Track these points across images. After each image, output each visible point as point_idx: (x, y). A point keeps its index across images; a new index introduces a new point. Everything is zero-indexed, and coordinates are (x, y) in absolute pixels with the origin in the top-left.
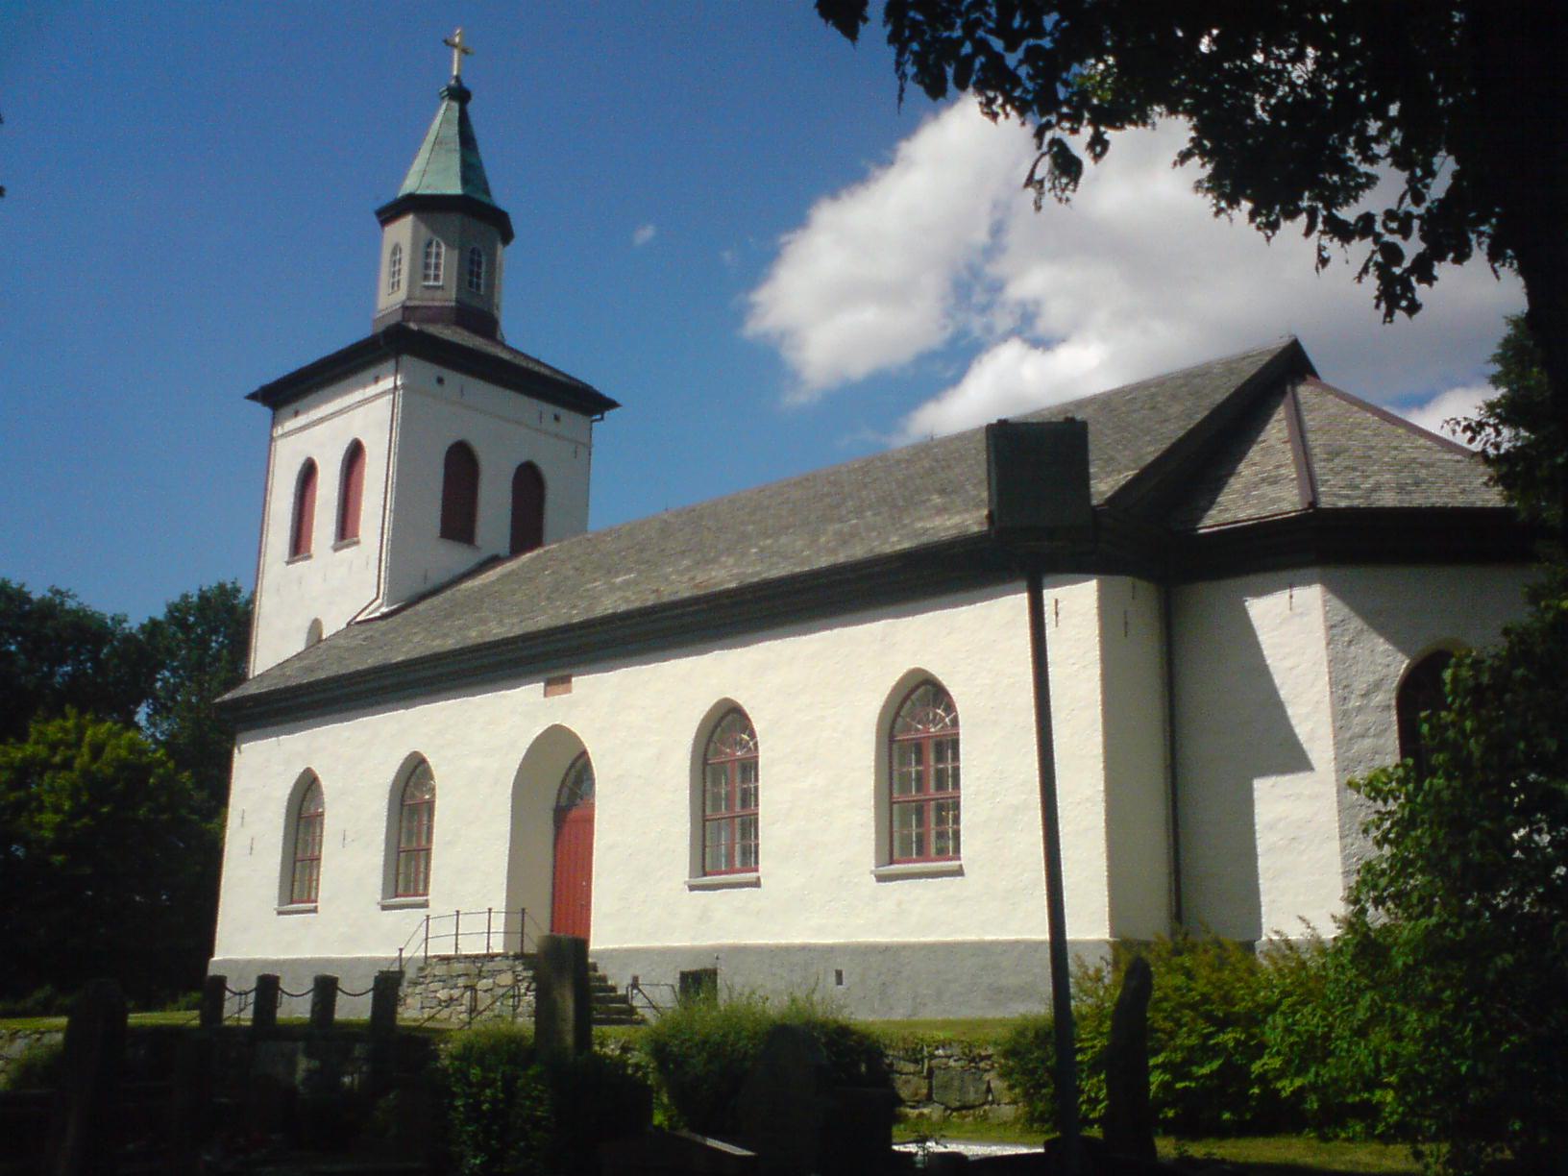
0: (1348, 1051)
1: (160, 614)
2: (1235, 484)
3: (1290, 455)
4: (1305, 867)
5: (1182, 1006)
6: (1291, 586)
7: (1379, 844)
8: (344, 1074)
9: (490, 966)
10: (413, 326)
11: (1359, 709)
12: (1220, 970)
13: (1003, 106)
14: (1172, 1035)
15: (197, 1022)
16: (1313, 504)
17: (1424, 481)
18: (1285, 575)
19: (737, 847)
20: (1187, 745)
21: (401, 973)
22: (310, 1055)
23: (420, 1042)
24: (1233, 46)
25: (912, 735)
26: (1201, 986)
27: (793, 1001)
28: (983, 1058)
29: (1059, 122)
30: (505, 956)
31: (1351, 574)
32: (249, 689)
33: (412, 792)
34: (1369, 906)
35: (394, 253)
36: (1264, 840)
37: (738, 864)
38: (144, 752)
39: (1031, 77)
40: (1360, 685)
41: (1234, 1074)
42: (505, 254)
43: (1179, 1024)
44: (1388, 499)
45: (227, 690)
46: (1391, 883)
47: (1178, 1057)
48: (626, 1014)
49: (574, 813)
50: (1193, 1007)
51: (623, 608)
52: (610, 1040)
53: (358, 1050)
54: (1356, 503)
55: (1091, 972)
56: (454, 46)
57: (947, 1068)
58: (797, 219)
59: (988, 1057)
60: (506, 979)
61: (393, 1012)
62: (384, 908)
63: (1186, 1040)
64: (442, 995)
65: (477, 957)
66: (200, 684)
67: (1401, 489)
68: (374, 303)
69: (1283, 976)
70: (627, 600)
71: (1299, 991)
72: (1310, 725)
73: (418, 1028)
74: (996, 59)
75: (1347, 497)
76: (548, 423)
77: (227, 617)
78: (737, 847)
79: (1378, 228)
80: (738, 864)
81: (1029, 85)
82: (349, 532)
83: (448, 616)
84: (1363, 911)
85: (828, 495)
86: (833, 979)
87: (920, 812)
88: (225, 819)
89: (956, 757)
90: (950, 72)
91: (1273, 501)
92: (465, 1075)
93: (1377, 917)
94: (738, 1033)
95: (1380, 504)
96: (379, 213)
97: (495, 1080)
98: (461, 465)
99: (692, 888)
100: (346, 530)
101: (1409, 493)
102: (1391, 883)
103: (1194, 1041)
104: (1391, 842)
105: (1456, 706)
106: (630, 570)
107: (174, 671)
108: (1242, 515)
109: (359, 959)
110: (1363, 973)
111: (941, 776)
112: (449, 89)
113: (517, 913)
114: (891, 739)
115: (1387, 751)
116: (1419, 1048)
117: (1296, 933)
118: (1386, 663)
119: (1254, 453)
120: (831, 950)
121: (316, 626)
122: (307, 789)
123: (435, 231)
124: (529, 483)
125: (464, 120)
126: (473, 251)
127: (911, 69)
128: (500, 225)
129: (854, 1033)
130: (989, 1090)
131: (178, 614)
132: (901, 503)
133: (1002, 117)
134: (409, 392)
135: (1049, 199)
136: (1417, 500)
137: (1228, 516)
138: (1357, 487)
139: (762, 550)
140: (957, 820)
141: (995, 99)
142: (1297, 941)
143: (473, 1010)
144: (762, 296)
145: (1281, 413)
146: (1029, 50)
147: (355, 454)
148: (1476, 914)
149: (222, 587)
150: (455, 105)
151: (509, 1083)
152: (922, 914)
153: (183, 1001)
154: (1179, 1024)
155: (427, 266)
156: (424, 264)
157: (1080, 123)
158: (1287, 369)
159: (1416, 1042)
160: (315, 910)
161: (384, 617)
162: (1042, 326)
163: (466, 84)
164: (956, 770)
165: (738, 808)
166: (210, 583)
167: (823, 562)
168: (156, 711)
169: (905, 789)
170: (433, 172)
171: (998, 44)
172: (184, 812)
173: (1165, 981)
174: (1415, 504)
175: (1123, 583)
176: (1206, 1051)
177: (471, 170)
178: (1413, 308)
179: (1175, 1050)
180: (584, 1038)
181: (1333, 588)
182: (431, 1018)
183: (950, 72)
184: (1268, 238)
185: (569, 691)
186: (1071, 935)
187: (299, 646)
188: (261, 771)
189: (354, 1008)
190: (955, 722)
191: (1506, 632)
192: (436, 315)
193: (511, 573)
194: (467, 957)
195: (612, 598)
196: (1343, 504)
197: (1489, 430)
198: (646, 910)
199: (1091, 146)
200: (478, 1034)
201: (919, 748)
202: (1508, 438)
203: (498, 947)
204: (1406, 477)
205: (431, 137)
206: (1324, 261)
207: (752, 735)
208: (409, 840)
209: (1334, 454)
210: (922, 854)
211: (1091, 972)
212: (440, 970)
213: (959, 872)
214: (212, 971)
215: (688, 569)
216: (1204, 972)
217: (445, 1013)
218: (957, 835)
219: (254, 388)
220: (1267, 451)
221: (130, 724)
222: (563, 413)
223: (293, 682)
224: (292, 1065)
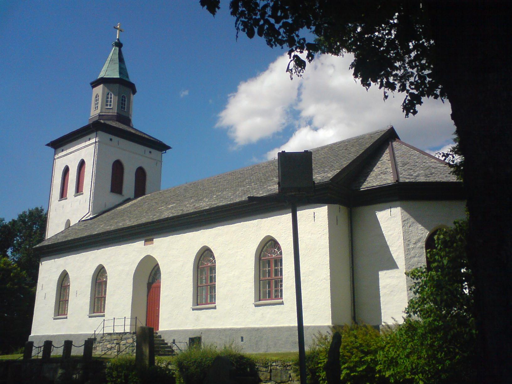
0: (403, 362)
1: (16, 218)
2: (373, 174)
3: (390, 165)
4: (394, 300)
5: (353, 348)
6: (391, 208)
7: (415, 293)
8: (73, 374)
9: (124, 337)
10: (102, 121)
11: (413, 248)
12: (366, 335)
13: (274, 42)
14: (350, 358)
15: (22, 358)
16: (397, 181)
17: (434, 173)
18: (388, 204)
19: (209, 296)
20: (356, 261)
21: (95, 339)
22: (62, 368)
23: (100, 362)
24: (369, 29)
25: (267, 258)
26: (359, 341)
27: (225, 347)
28: (288, 366)
29: (296, 49)
30: (130, 333)
31: (405, 203)
32: (45, 243)
33: (100, 278)
34: (412, 314)
35: (96, 97)
36: (383, 292)
37: (209, 301)
38: (10, 265)
39: (284, 33)
40: (413, 241)
41: (370, 370)
42: (133, 98)
43: (352, 354)
44: (422, 179)
45: (38, 243)
46: (419, 306)
47: (352, 365)
48: (170, 351)
49: (154, 285)
50: (357, 348)
51: (171, 215)
52: (162, 361)
53: (79, 366)
54: (411, 180)
55: (324, 337)
56: (117, 29)
57: (277, 369)
58: (234, 89)
59: (290, 365)
60: (130, 341)
61: (91, 353)
62: (90, 317)
63: (355, 359)
64: (109, 346)
65: (120, 333)
66: (30, 241)
67: (426, 176)
68: (90, 113)
69: (387, 337)
70: (172, 213)
71: (392, 342)
72: (397, 254)
73: (100, 358)
74: (271, 26)
75: (409, 178)
76: (147, 154)
77: (39, 219)
78: (209, 296)
79: (408, 88)
80: (209, 301)
81: (284, 35)
82: (80, 190)
83: (112, 219)
84: (410, 316)
85: (240, 178)
86: (240, 340)
87: (269, 284)
88: (36, 287)
89: (281, 265)
90: (256, 30)
91: (385, 180)
92: (112, 374)
93: (415, 317)
94: (206, 359)
95: (420, 181)
96: (91, 84)
97: (122, 376)
98: (118, 168)
99: (193, 310)
100: (79, 190)
101: (429, 177)
102: (419, 306)
103: (357, 359)
104: (419, 293)
105: (439, 248)
106: (174, 203)
107: (21, 237)
108: (375, 185)
109: (81, 334)
110: (409, 337)
111: (276, 271)
112: (116, 43)
113: (134, 319)
114: (260, 259)
115: (422, 262)
116: (427, 361)
117: (391, 322)
118: (422, 233)
119: (379, 164)
120: (240, 330)
121: (68, 221)
122: (64, 278)
123: (109, 90)
124: (141, 174)
125: (120, 53)
126: (123, 96)
127: (241, 27)
128: (132, 88)
129: (245, 358)
130: (290, 376)
131: (22, 217)
132: (263, 181)
133: (274, 46)
134: (100, 143)
135: (294, 76)
136: (431, 179)
137: (370, 185)
138: (412, 175)
139: (217, 196)
140: (281, 286)
141: (271, 40)
142: (391, 325)
143: (119, 351)
144: (223, 114)
145: (387, 151)
146: (283, 23)
147: (82, 164)
148: (445, 316)
149: (37, 209)
150: (118, 48)
151: (126, 376)
152: (281, 316)
153: (20, 350)
154: (352, 354)
155: (107, 101)
156: (106, 101)
157: (303, 49)
158: (390, 136)
159: (425, 359)
160: (66, 318)
161: (91, 219)
162: (316, 123)
163: (121, 41)
164: (281, 269)
165: (209, 282)
166: (32, 207)
167: (238, 200)
168: (14, 251)
169: (264, 276)
170: (109, 70)
171: (272, 21)
172: (23, 285)
173: (346, 340)
174: (430, 181)
175: (336, 207)
176: (361, 363)
177: (122, 70)
178: (415, 112)
179: (351, 362)
180: (152, 361)
181: (404, 208)
182: (105, 354)
183: (256, 30)
184: (367, 89)
185: (153, 243)
186: (305, 324)
187: (63, 228)
188: (49, 271)
189: (77, 351)
190: (281, 253)
191: (455, 223)
192: (110, 118)
193: (135, 205)
194: (117, 333)
195: (168, 212)
196: (407, 181)
197: (450, 156)
198: (178, 317)
199: (308, 57)
200: (119, 359)
201: (269, 262)
202: (458, 159)
203: (128, 330)
204: (427, 172)
205: (109, 59)
206: (386, 97)
207: (214, 258)
208: (99, 294)
209: (404, 164)
210: (270, 297)
211: (324, 337)
212: (108, 338)
213: (282, 303)
214: (30, 340)
215: (193, 203)
216: (361, 336)
217: (110, 352)
218: (281, 291)
219: (49, 142)
220: (383, 164)
221: (5, 255)
222: (153, 151)
223: (60, 241)
224: (56, 372)
